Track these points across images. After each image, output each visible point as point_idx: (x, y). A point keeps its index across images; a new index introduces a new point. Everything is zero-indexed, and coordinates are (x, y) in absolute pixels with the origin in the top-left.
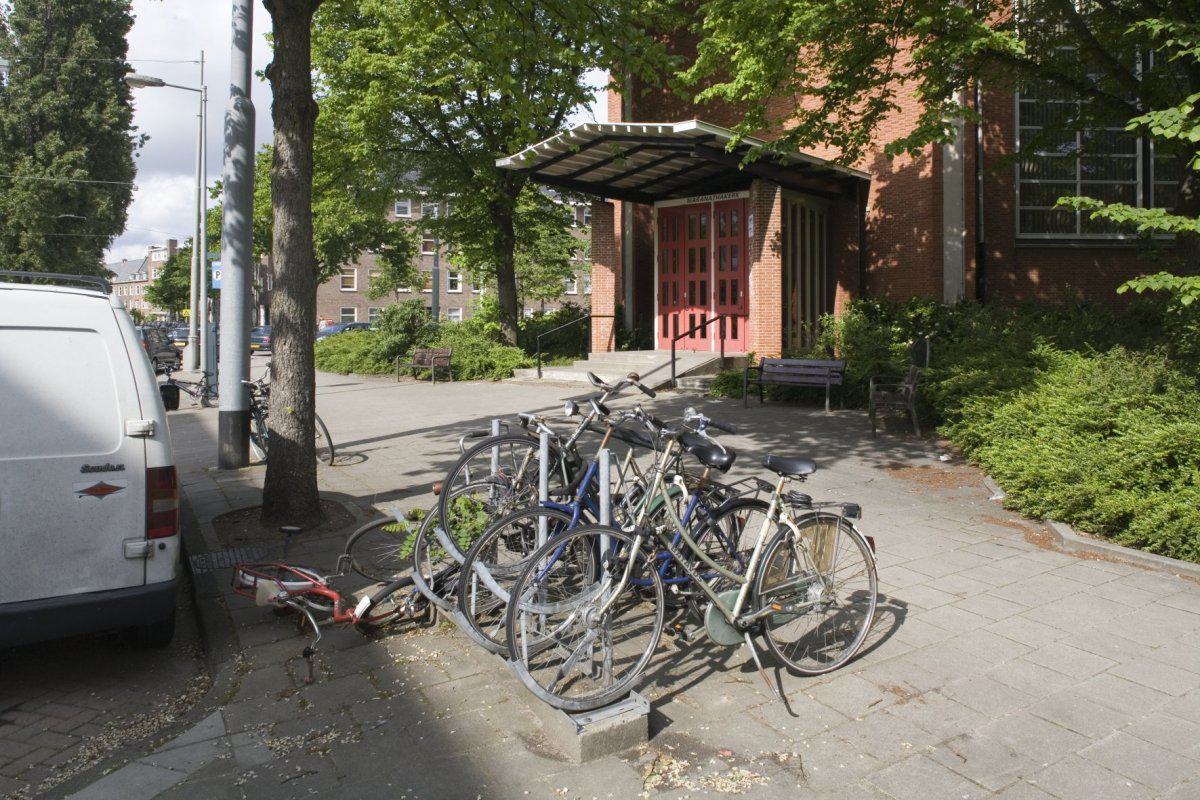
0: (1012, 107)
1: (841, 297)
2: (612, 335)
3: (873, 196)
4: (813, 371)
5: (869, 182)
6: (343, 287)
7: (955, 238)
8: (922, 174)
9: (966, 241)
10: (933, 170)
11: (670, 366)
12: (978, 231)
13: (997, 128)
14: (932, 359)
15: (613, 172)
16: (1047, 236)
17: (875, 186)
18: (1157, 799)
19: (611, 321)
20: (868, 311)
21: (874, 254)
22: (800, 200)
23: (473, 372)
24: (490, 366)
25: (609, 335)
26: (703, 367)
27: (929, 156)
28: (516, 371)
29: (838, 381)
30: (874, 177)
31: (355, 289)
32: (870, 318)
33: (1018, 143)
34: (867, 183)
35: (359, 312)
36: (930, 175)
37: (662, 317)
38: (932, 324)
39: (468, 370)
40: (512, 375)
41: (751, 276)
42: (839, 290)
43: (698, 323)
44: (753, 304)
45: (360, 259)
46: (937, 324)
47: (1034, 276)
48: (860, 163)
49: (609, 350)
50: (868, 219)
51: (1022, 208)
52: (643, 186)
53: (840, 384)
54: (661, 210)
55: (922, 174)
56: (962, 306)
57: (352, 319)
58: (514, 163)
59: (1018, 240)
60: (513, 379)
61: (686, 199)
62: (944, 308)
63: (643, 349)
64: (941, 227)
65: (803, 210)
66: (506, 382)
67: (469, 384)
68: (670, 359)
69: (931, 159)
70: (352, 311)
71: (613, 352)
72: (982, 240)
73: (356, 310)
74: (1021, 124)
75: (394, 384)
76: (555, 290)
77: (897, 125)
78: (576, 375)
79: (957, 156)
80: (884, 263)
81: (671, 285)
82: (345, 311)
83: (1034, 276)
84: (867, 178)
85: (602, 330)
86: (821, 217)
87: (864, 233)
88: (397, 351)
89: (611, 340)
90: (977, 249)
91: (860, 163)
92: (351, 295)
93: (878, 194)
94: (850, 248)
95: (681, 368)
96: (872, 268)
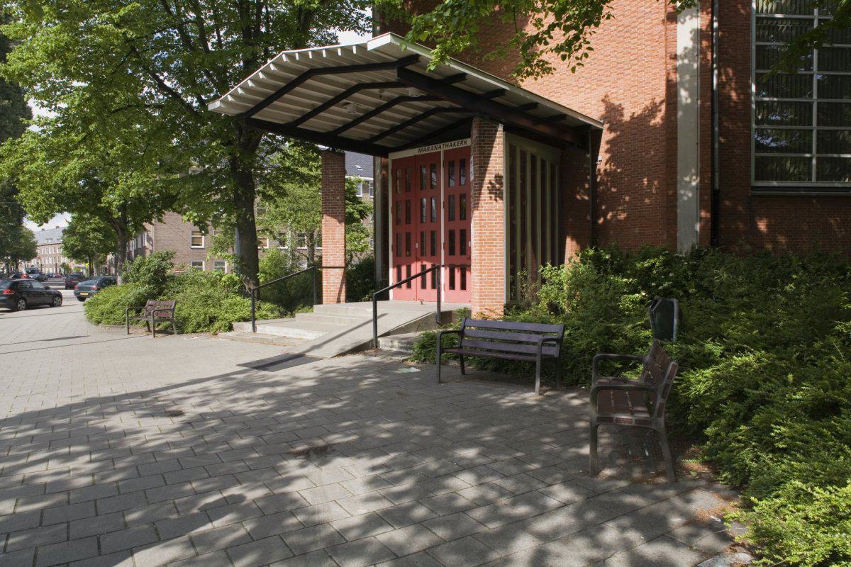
0: (749, 50)
1: (571, 246)
2: (341, 286)
3: (603, 146)
4: (523, 337)
5: (601, 131)
6: (193, 245)
7: (690, 183)
8: (653, 122)
9: (701, 188)
10: (664, 119)
11: (371, 324)
12: (713, 178)
13: (730, 71)
14: (682, 326)
15: (342, 121)
16: (775, 184)
17: (607, 136)
18: (472, 3)
19: (341, 272)
20: (597, 260)
21: (603, 207)
22: (531, 149)
23: (199, 325)
24: (212, 320)
25: (339, 286)
26: (415, 323)
27: (661, 103)
28: (235, 324)
29: (553, 351)
30: (606, 126)
31: (203, 247)
32: (599, 269)
33: (754, 88)
34: (599, 133)
35: (206, 265)
36: (660, 122)
37: (396, 269)
38: (666, 274)
39: (195, 322)
40: (231, 328)
41: (472, 225)
42: (568, 240)
43: (429, 275)
44: (474, 254)
45: (164, 218)
46: (671, 275)
47: (762, 226)
48: (586, 55)
49: (339, 301)
50: (599, 170)
51: (758, 155)
52: (377, 138)
53: (556, 355)
54: (394, 161)
55: (653, 122)
56: (696, 254)
57: (201, 269)
58: (223, 106)
59: (752, 187)
60: (230, 334)
61: (417, 149)
62: (677, 257)
63: (385, 300)
64: (675, 173)
65: (533, 158)
66: (224, 335)
67: (195, 337)
68: (371, 316)
69: (663, 107)
70: (200, 264)
71: (343, 303)
72: (717, 186)
73: (204, 263)
74: (757, 67)
75: (123, 337)
76: (360, 247)
77: (629, 72)
78: (285, 330)
79: (689, 101)
80: (613, 216)
81: (403, 237)
82: (194, 264)
83: (762, 226)
84: (601, 127)
85: (332, 281)
86: (552, 167)
87: (595, 184)
88: (139, 305)
89: (340, 291)
90: (712, 198)
91: (586, 55)
92: (199, 251)
93: (609, 146)
94: (578, 197)
95: (384, 326)
96: (601, 221)
